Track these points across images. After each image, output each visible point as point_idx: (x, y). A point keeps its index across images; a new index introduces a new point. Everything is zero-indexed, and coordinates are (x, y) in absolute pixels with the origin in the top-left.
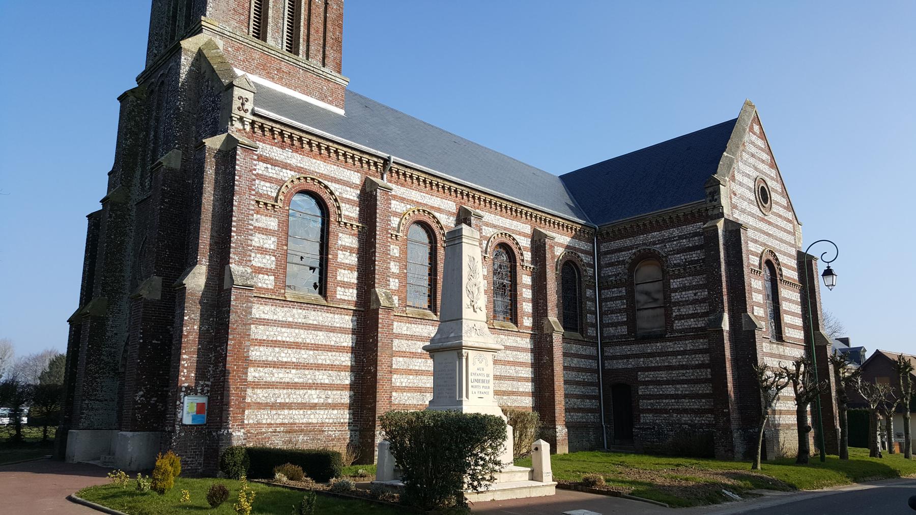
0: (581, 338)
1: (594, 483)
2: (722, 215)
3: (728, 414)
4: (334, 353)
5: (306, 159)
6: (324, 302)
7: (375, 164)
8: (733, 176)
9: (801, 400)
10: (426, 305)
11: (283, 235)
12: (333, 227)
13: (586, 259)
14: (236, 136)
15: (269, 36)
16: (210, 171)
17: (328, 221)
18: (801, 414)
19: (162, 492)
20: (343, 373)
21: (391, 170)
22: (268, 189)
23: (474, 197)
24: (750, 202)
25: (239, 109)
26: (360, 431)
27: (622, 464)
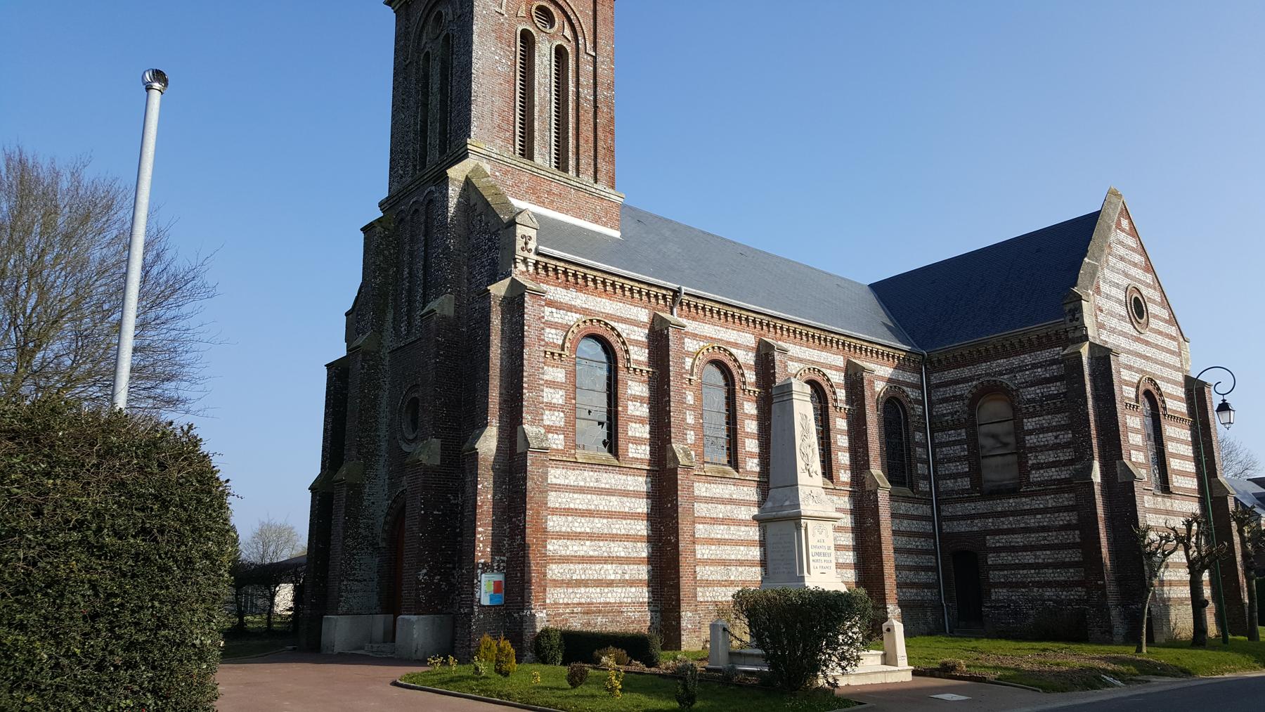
0: (911, 494)
1: (953, 668)
2: (1086, 338)
3: (1104, 586)
5: (591, 298)
6: (616, 463)
7: (664, 297)
8: (1098, 288)
9: (1195, 568)
10: (725, 460)
11: (570, 387)
12: (622, 374)
13: (913, 394)
14: (520, 279)
15: (536, 152)
16: (496, 321)
17: (616, 367)
18: (1195, 585)
19: (506, 674)
20: (639, 544)
21: (681, 304)
22: (553, 336)
23: (775, 327)
24: (1121, 318)
26: (661, 612)
27: (975, 649)
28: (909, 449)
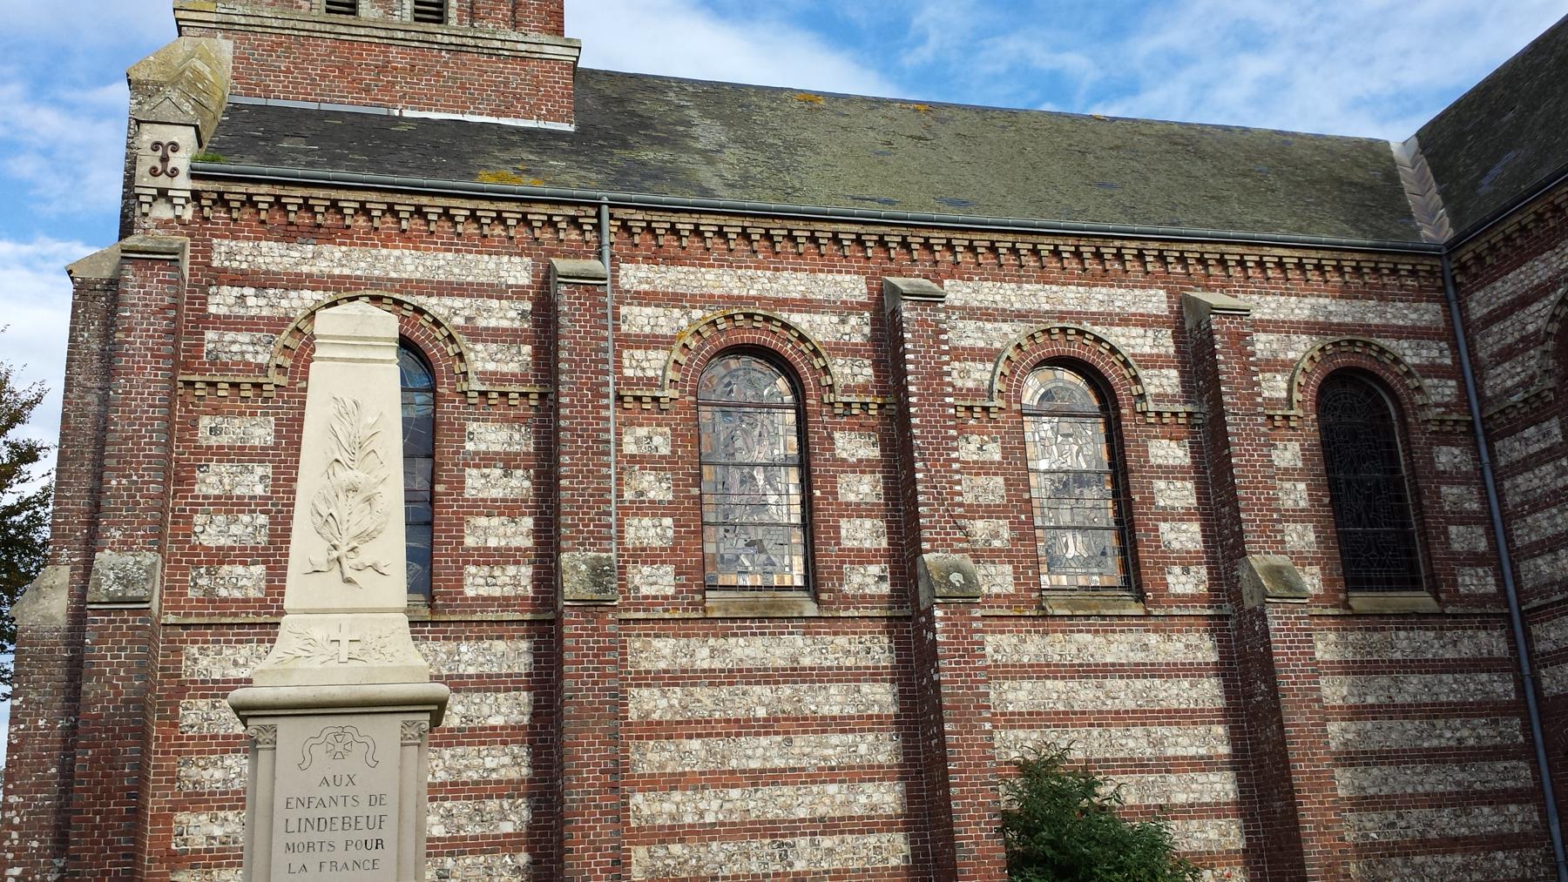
4: (459, 750)
5: (356, 253)
25: (154, 172)
28: (1418, 493)
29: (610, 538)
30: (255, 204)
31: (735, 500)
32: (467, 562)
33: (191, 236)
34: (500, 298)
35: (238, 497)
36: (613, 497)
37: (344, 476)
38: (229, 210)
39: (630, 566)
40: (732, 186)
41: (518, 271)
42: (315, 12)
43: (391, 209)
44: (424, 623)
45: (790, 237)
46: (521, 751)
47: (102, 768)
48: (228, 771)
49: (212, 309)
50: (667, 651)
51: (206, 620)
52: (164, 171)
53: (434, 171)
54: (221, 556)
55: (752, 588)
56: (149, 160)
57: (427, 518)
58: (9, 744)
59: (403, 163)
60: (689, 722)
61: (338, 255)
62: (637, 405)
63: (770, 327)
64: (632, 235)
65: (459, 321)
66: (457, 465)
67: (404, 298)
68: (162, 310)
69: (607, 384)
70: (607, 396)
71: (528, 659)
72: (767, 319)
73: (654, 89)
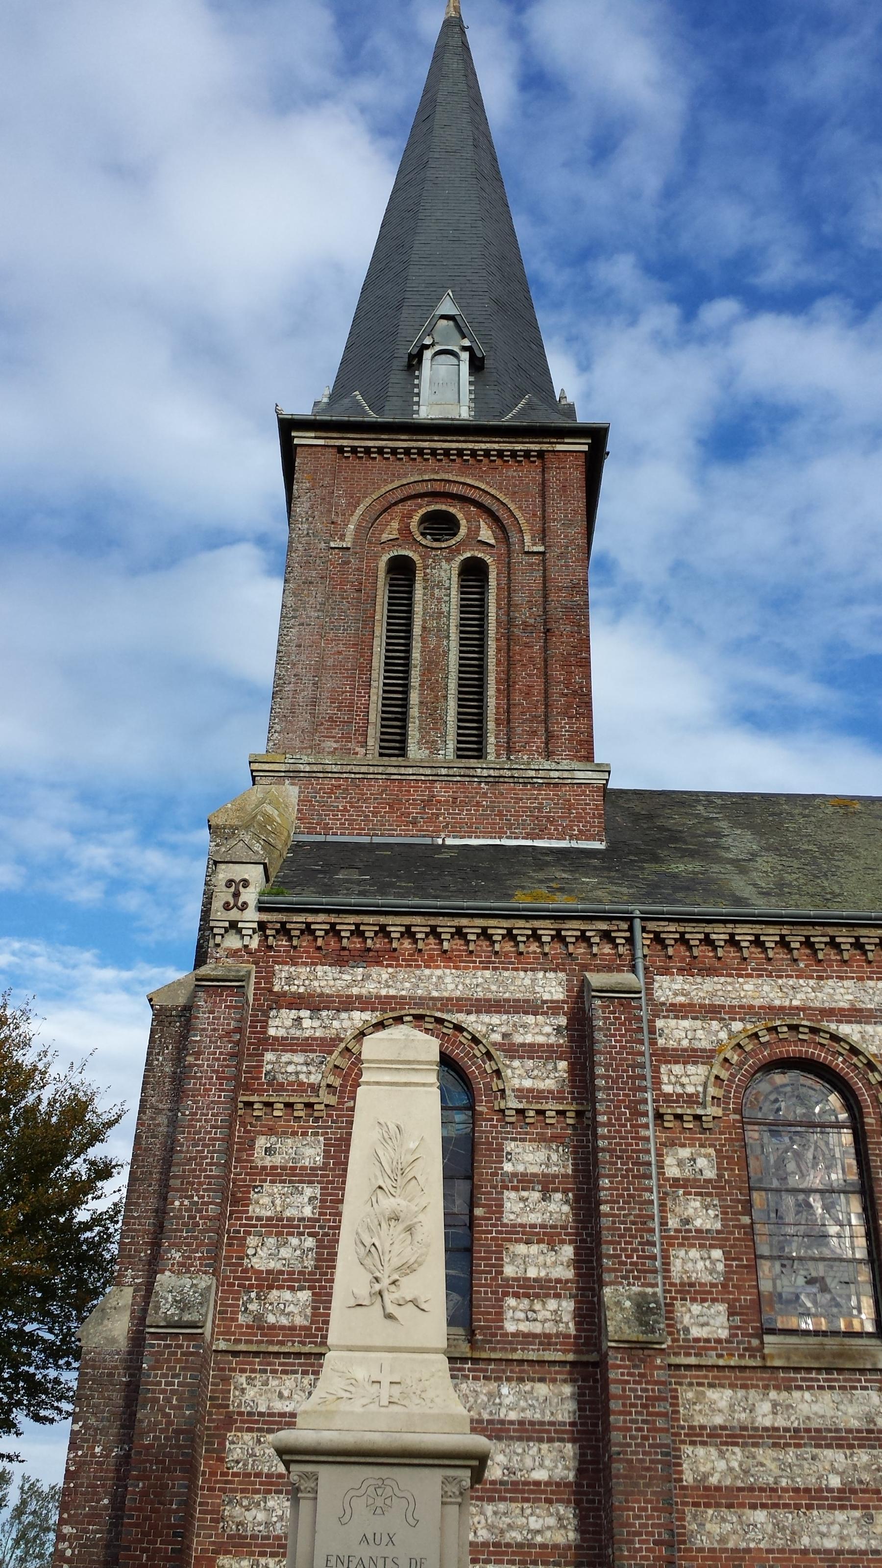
4: (502, 1506)
25: (227, 907)
29: (655, 1272)
30: (312, 932)
31: (791, 1230)
32: (506, 1294)
33: (256, 963)
34: (535, 1014)
35: (289, 1219)
36: (656, 1225)
37: (387, 1204)
38: (290, 939)
39: (678, 1303)
40: (767, 894)
41: (552, 987)
42: (369, 756)
43: (434, 932)
44: (464, 1360)
45: (833, 944)
46: (567, 1512)
47: (152, 1502)
48: (266, 1514)
49: (272, 1032)
50: (723, 1404)
51: (254, 1348)
52: (236, 905)
53: (473, 893)
54: (270, 1281)
55: (816, 1333)
56: (223, 896)
57: (466, 1246)
58: (67, 1470)
59: (445, 888)
60: (751, 1489)
61: (385, 976)
62: (678, 1123)
63: (817, 1039)
64: (665, 947)
65: (496, 1037)
66: (495, 1187)
67: (445, 1016)
68: (228, 1033)
69: (645, 1101)
70: (646, 1114)
71: (571, 1406)
72: (814, 1031)
73: (682, 804)
